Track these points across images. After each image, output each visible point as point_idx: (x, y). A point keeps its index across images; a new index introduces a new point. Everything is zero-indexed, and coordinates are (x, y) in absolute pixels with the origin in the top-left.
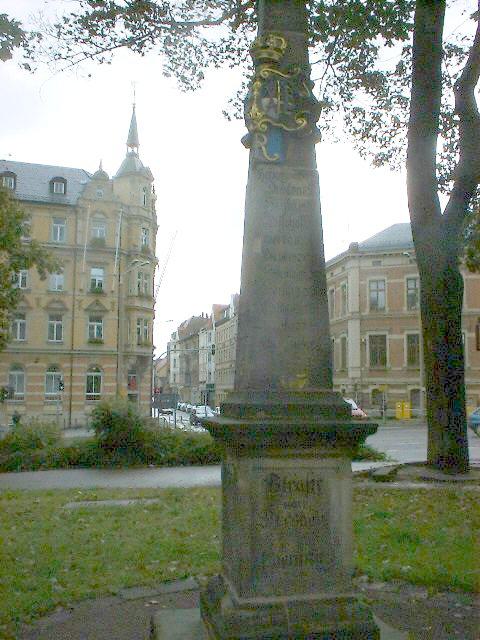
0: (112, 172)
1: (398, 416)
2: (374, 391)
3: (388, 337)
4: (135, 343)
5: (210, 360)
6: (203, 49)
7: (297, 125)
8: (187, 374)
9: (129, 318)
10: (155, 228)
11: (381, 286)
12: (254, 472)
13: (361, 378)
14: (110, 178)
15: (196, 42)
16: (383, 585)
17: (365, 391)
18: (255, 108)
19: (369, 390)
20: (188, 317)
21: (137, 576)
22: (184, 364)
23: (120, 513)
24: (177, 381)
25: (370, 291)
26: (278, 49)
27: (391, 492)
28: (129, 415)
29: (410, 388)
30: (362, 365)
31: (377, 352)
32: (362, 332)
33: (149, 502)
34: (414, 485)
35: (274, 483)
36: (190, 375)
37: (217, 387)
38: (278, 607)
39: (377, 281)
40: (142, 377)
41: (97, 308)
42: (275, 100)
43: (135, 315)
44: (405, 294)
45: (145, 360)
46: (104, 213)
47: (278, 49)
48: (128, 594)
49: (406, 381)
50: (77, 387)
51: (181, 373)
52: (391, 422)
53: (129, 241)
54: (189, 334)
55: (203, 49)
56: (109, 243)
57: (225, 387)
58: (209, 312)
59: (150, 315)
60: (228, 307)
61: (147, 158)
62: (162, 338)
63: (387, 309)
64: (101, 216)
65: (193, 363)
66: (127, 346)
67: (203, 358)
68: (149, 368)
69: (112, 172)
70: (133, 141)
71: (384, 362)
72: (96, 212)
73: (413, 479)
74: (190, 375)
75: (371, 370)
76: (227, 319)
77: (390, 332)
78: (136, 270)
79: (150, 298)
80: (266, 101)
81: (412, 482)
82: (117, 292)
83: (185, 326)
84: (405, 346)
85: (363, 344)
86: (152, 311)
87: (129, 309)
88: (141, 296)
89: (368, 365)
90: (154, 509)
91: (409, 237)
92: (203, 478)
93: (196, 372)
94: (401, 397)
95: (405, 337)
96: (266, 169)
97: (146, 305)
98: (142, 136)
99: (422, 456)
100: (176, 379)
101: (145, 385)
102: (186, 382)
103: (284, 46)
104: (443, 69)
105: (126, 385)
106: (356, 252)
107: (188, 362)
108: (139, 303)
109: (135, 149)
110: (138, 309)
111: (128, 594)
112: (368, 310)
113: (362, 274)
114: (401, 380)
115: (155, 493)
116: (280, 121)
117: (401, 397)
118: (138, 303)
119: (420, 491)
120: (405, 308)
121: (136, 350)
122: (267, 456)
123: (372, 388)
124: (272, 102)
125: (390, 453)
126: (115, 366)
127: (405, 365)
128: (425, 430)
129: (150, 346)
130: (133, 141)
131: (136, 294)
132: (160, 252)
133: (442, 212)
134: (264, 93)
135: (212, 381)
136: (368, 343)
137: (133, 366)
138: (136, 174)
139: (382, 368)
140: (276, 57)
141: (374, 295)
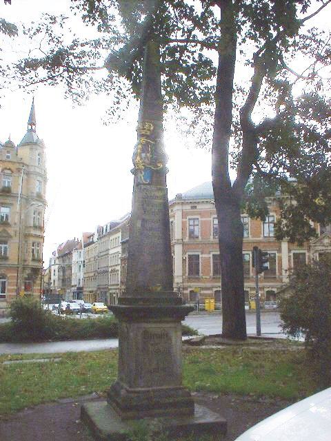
0: (17, 142)
1: (206, 308)
2: (190, 292)
3: (200, 256)
4: (31, 259)
5: (80, 270)
6: (90, 82)
7: (158, 167)
8: (63, 281)
9: (26, 241)
10: (45, 180)
11: (196, 223)
12: (135, 331)
13: (183, 282)
14: (16, 146)
15: (87, 79)
16: (195, 393)
17: (185, 292)
18: (138, 158)
19: (187, 292)
20: (64, 241)
21: (64, 393)
22: (61, 274)
23: (41, 366)
24: (56, 285)
25: (190, 225)
26: (149, 130)
27: (201, 351)
28: (36, 307)
29: (215, 289)
30: (184, 274)
31: (193, 265)
32: (184, 252)
33: (57, 360)
34: (214, 347)
35: (147, 335)
36: (65, 280)
37: (85, 289)
38: (148, 391)
39: (194, 219)
40: (34, 282)
41: (4, 235)
42: (148, 154)
43: (31, 240)
44: (212, 227)
45: (36, 271)
46: (9, 169)
47: (149, 130)
48: (61, 401)
49: (209, 285)
50: (13, 286)
51: (59, 279)
52: (202, 313)
53: (28, 189)
54: (65, 254)
55: (90, 82)
56: (14, 191)
57: (90, 289)
58: (80, 238)
59: (41, 240)
60: (93, 235)
61: (41, 133)
62: (48, 253)
63: (200, 237)
64: (9, 172)
65: (67, 273)
66: (25, 261)
67: (75, 269)
68: (40, 276)
69: (17, 142)
70: (32, 122)
71: (198, 273)
72: (6, 169)
73: (213, 343)
74: (65, 280)
75: (189, 278)
76: (93, 242)
77: (202, 253)
78: (32, 209)
79: (41, 228)
80: (143, 155)
81: (213, 345)
82: (18, 223)
83: (62, 247)
84: (212, 265)
85: (184, 260)
86: (43, 238)
87: (27, 236)
88: (35, 227)
89: (187, 274)
90: (61, 363)
91: (211, 191)
92: (85, 347)
93: (70, 279)
94: (210, 296)
95: (211, 256)
96: (143, 187)
97: (38, 233)
98: (38, 118)
99: (219, 331)
100: (56, 285)
101: (37, 288)
102: (63, 286)
103: (152, 128)
104: (233, 100)
105: (23, 287)
106: (179, 197)
107: (64, 271)
108: (33, 234)
109: (34, 127)
110: (32, 236)
111: (61, 401)
112: (187, 238)
113: (184, 215)
114: (209, 285)
115: (57, 355)
116: (150, 164)
117: (210, 296)
118: (33, 232)
119: (217, 350)
120: (212, 237)
121: (31, 264)
122: (144, 322)
123: (189, 289)
124: (146, 155)
125: (200, 331)
126: (16, 275)
127: (211, 274)
128: (221, 317)
129: (40, 261)
130: (32, 122)
131: (32, 225)
132: (49, 197)
133: (232, 185)
134: (143, 151)
135: (81, 285)
136: (187, 260)
137: (28, 275)
138: (31, 142)
139: (197, 276)
140: (148, 133)
141: (192, 228)
